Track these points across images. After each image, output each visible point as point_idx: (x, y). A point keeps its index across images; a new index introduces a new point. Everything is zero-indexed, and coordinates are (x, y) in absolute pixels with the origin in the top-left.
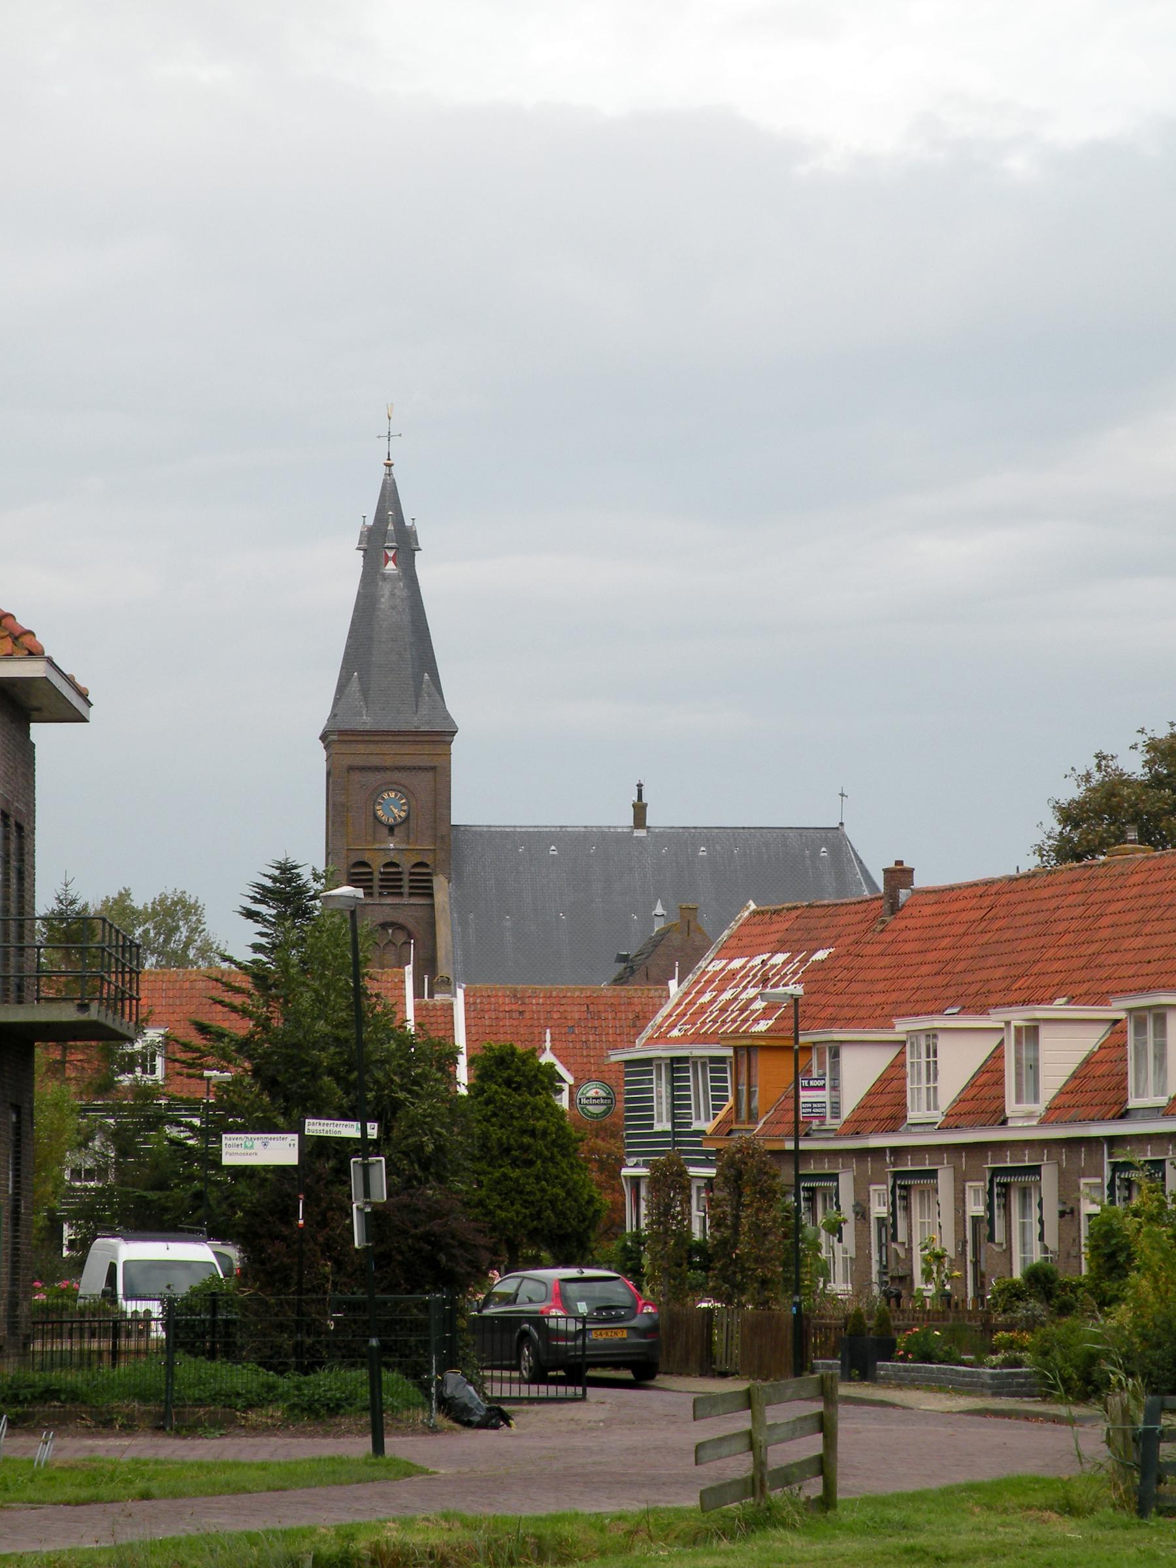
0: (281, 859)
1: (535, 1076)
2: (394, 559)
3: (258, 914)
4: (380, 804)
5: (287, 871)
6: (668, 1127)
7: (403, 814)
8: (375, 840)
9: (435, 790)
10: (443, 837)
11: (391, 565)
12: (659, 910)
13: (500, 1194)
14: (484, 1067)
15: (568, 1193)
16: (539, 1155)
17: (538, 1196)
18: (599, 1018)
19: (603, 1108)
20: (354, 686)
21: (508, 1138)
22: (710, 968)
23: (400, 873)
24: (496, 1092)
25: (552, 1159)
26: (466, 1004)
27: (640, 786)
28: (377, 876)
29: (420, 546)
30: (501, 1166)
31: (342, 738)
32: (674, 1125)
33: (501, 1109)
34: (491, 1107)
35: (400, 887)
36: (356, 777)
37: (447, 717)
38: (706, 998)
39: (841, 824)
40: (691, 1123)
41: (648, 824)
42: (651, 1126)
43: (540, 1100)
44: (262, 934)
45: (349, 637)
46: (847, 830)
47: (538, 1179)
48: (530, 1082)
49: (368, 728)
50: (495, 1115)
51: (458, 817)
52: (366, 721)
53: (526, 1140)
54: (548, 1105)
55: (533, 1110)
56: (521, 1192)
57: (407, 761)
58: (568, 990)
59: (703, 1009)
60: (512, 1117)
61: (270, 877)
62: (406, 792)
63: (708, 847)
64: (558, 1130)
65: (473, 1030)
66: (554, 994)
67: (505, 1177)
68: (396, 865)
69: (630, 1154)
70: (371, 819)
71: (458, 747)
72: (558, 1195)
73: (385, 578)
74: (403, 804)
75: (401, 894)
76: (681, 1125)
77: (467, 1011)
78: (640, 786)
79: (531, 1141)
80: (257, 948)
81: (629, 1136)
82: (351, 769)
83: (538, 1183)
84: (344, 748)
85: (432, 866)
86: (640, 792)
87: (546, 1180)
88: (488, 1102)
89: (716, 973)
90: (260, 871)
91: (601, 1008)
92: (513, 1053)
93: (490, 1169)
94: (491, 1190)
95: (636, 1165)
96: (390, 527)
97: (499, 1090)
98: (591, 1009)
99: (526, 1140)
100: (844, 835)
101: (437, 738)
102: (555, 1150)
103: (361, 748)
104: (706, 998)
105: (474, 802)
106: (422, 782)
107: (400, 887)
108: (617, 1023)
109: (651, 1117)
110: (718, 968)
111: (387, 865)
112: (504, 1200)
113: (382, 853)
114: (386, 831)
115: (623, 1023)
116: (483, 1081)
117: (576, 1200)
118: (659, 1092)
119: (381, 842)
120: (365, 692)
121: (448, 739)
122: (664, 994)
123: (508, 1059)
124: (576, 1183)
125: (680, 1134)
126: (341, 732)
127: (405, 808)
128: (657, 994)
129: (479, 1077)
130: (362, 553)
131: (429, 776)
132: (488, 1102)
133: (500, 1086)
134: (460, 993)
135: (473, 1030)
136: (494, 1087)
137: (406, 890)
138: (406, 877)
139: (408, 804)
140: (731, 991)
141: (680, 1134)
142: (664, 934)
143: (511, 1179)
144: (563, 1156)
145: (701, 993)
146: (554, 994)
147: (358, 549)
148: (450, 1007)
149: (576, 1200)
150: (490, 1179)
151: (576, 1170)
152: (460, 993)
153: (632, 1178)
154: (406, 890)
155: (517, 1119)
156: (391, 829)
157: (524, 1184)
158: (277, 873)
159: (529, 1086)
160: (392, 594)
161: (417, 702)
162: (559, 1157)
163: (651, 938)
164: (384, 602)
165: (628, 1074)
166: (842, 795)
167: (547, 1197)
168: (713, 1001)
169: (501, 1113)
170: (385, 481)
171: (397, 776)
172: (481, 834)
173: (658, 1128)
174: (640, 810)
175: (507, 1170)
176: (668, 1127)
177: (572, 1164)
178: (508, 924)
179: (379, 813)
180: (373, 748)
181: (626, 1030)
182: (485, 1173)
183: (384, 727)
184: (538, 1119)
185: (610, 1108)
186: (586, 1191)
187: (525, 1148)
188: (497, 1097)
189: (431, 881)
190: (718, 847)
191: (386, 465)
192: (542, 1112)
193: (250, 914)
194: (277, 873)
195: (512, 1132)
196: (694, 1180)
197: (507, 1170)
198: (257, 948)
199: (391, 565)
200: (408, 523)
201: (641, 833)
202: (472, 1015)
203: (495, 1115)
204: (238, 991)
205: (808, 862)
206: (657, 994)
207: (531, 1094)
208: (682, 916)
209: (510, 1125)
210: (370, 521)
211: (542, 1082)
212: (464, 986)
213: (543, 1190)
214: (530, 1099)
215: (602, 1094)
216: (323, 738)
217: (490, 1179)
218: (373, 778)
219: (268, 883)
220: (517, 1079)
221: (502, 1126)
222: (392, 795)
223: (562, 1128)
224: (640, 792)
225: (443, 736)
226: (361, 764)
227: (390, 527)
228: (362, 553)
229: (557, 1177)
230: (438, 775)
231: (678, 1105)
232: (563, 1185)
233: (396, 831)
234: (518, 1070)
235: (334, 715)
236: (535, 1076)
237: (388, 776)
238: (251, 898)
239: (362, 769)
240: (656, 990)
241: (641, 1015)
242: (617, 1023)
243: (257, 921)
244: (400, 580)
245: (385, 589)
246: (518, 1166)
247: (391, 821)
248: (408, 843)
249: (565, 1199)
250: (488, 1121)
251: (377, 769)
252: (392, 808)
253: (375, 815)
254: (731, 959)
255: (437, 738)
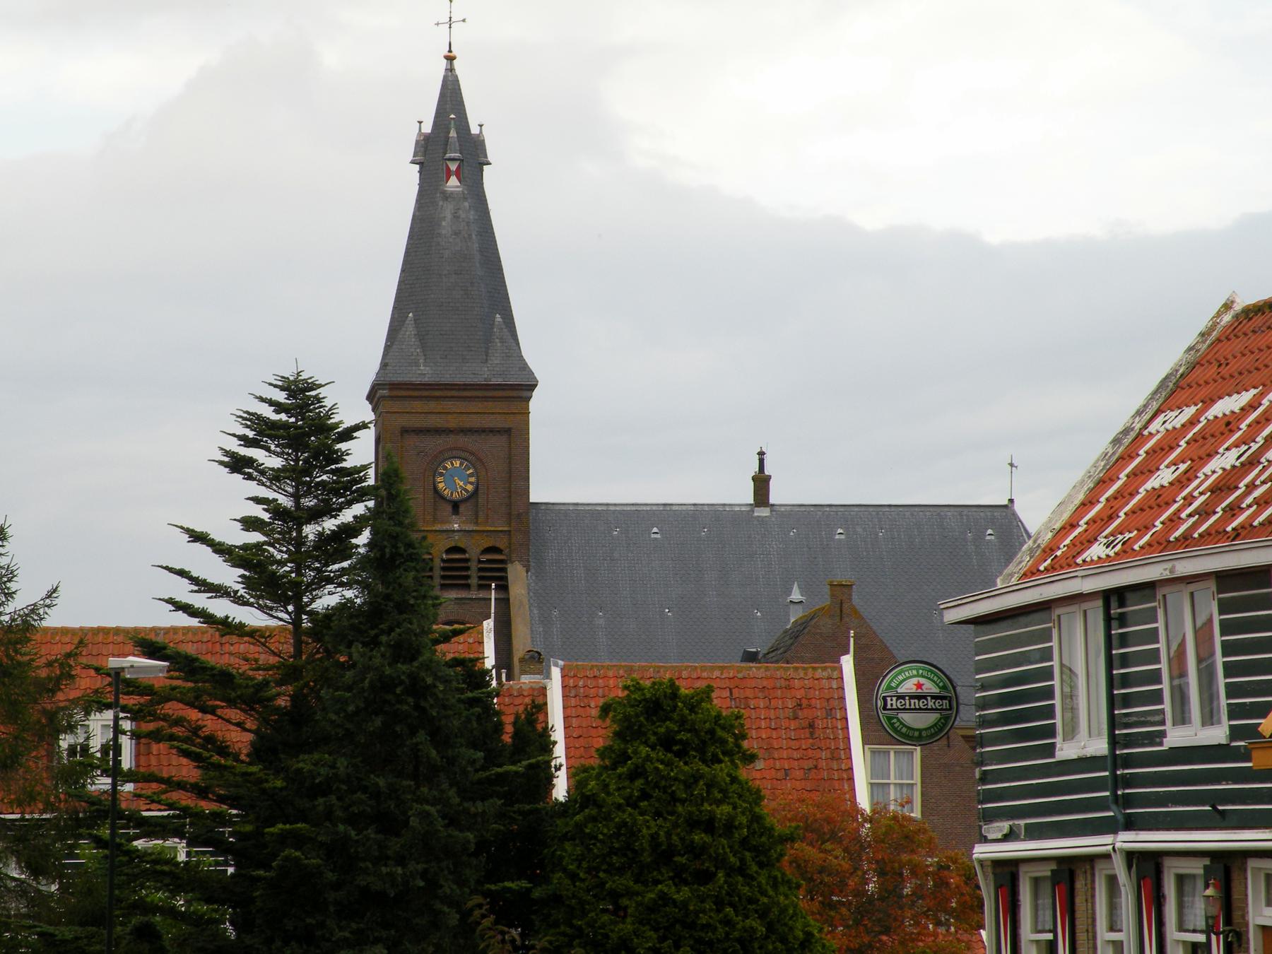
0: (289, 373)
1: (712, 732)
2: (458, 173)
3: (250, 462)
4: (441, 474)
5: (300, 393)
6: (1099, 746)
7: (470, 488)
8: (435, 520)
9: (510, 472)
10: (519, 515)
11: (453, 181)
12: (796, 595)
13: (656, 930)
14: (627, 718)
15: (770, 928)
16: (721, 862)
17: (721, 931)
18: (747, 707)
19: (932, 718)
20: (410, 329)
21: (669, 835)
22: (1153, 428)
23: (467, 560)
24: (648, 758)
25: (742, 870)
26: (564, 687)
27: (761, 454)
28: (437, 563)
29: (490, 158)
30: (657, 882)
31: (395, 393)
32: (1114, 741)
33: (657, 786)
34: (639, 783)
35: (467, 577)
36: (412, 441)
37: (524, 367)
38: (1165, 476)
39: (1011, 501)
40: (1163, 734)
41: (772, 501)
42: (1050, 750)
43: (721, 771)
44: (257, 500)
45: (403, 271)
46: (1018, 507)
47: (719, 904)
48: (704, 742)
49: (426, 380)
50: (645, 796)
51: (538, 494)
52: (424, 372)
53: (698, 837)
54: (734, 780)
55: (709, 786)
56: (692, 926)
57: (475, 422)
58: (703, 669)
59: (1160, 499)
60: (674, 799)
61: (271, 403)
62: (475, 460)
63: (846, 529)
64: (751, 822)
65: (575, 722)
66: (685, 674)
67: (664, 898)
68: (462, 551)
69: (990, 816)
70: (431, 493)
71: (538, 405)
72: (753, 930)
73: (447, 196)
74: (471, 475)
75: (467, 587)
76: (1130, 741)
77: (565, 697)
78: (761, 454)
79: (707, 839)
80: (250, 524)
81: (985, 778)
82: (405, 431)
83: (718, 911)
84: (397, 406)
85: (506, 551)
86: (761, 462)
87: (731, 905)
88: (634, 775)
89: (1172, 438)
90: (253, 389)
91: (749, 693)
92: (675, 695)
93: (638, 887)
94: (641, 923)
95: (1009, 837)
96: (453, 134)
97: (653, 755)
98: (736, 693)
99: (698, 837)
100: (1014, 514)
101: (515, 394)
102: (748, 854)
103: (418, 406)
104: (1165, 476)
105: (559, 473)
106: (492, 447)
107: (467, 577)
108: (772, 714)
109: (1050, 731)
110: (1178, 423)
111: (449, 551)
112: (663, 939)
113: (445, 536)
114: (449, 508)
115: (781, 714)
116: (625, 741)
117: (784, 940)
118: (1068, 672)
119: (443, 522)
120: (422, 338)
121: (525, 394)
122: (835, 675)
123: (667, 704)
124: (783, 911)
125: (1128, 761)
126: (394, 386)
127: (473, 479)
128: (825, 674)
129: (618, 735)
130: (417, 167)
131: (502, 440)
132: (634, 775)
133: (653, 748)
134: (556, 673)
135: (575, 722)
136: (644, 750)
137: (474, 581)
138: (474, 565)
139: (476, 474)
140: (1234, 453)
141: (1128, 761)
142: (803, 624)
143: (674, 902)
144: (761, 865)
145: (1147, 470)
146: (685, 674)
147: (413, 162)
148: (543, 691)
149: (784, 940)
150: (639, 904)
151: (782, 889)
152: (556, 673)
153: (998, 864)
154: (474, 581)
155: (683, 801)
156: (456, 506)
157: (697, 913)
158: (281, 397)
159: (702, 750)
160: (456, 217)
161: (488, 348)
162: (755, 868)
163: (786, 631)
164: (446, 226)
165: (982, 648)
166: (1011, 465)
167: (736, 934)
168: (1181, 482)
169: (656, 793)
170: (445, 77)
171: (462, 440)
172: (566, 513)
173: (1066, 751)
174: (761, 483)
175: (666, 887)
176: (1099, 746)
177: (775, 878)
178: (602, 622)
179: (441, 486)
180: (432, 405)
181: (784, 724)
182: (630, 894)
183: (447, 379)
184: (719, 803)
185: (947, 718)
186: (799, 925)
187: (696, 852)
188: (649, 766)
189: (504, 570)
190: (859, 530)
191: (447, 58)
192: (723, 791)
193: (237, 464)
194: (281, 397)
195: (676, 825)
196: (1168, 863)
197: (666, 887)
198: (250, 524)
199: (453, 181)
200: (474, 130)
201: (763, 512)
202: (573, 702)
203: (645, 796)
204: (218, 591)
205: (971, 548)
206: (825, 674)
207: (704, 761)
208: (833, 596)
209: (672, 813)
210: (427, 128)
211: (723, 742)
212: (561, 663)
213: (727, 922)
214: (704, 769)
215: (930, 687)
216: (370, 397)
217: (639, 904)
218: (433, 444)
219: (268, 412)
220: (683, 736)
221: (658, 814)
222: (457, 463)
223: (757, 819)
224: (761, 462)
225: (520, 390)
226: (418, 425)
227: (453, 134)
228: (417, 167)
229: (751, 901)
230: (514, 438)
231: (1125, 691)
232: (763, 914)
233: (462, 508)
234: (683, 721)
235: (384, 365)
236: (712, 732)
237: (451, 440)
238: (240, 438)
239: (419, 431)
240: (825, 669)
241: (805, 703)
242: (772, 714)
243: (249, 477)
244: (465, 199)
245: (448, 210)
246: (686, 883)
247: (456, 496)
248: (477, 523)
249: (767, 937)
250: (635, 806)
251: (438, 431)
252: (456, 480)
253: (435, 488)
254: (1209, 402)
255: (515, 394)
